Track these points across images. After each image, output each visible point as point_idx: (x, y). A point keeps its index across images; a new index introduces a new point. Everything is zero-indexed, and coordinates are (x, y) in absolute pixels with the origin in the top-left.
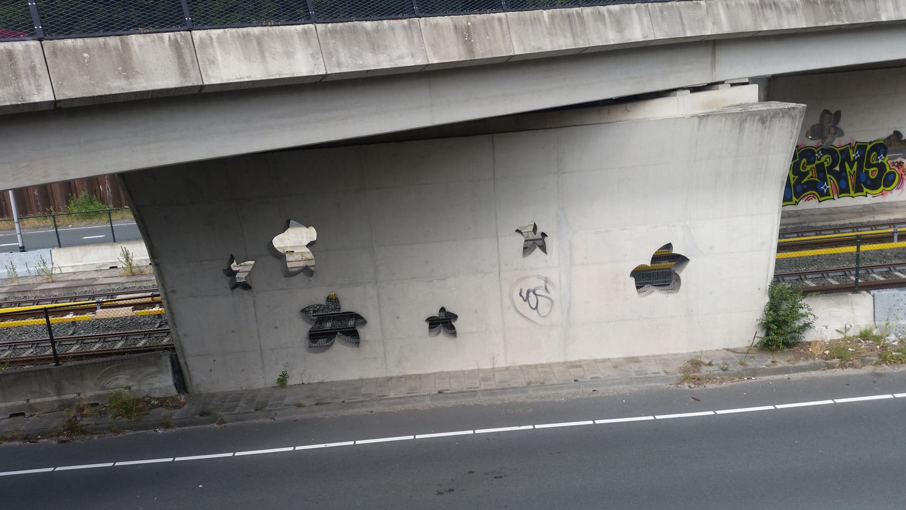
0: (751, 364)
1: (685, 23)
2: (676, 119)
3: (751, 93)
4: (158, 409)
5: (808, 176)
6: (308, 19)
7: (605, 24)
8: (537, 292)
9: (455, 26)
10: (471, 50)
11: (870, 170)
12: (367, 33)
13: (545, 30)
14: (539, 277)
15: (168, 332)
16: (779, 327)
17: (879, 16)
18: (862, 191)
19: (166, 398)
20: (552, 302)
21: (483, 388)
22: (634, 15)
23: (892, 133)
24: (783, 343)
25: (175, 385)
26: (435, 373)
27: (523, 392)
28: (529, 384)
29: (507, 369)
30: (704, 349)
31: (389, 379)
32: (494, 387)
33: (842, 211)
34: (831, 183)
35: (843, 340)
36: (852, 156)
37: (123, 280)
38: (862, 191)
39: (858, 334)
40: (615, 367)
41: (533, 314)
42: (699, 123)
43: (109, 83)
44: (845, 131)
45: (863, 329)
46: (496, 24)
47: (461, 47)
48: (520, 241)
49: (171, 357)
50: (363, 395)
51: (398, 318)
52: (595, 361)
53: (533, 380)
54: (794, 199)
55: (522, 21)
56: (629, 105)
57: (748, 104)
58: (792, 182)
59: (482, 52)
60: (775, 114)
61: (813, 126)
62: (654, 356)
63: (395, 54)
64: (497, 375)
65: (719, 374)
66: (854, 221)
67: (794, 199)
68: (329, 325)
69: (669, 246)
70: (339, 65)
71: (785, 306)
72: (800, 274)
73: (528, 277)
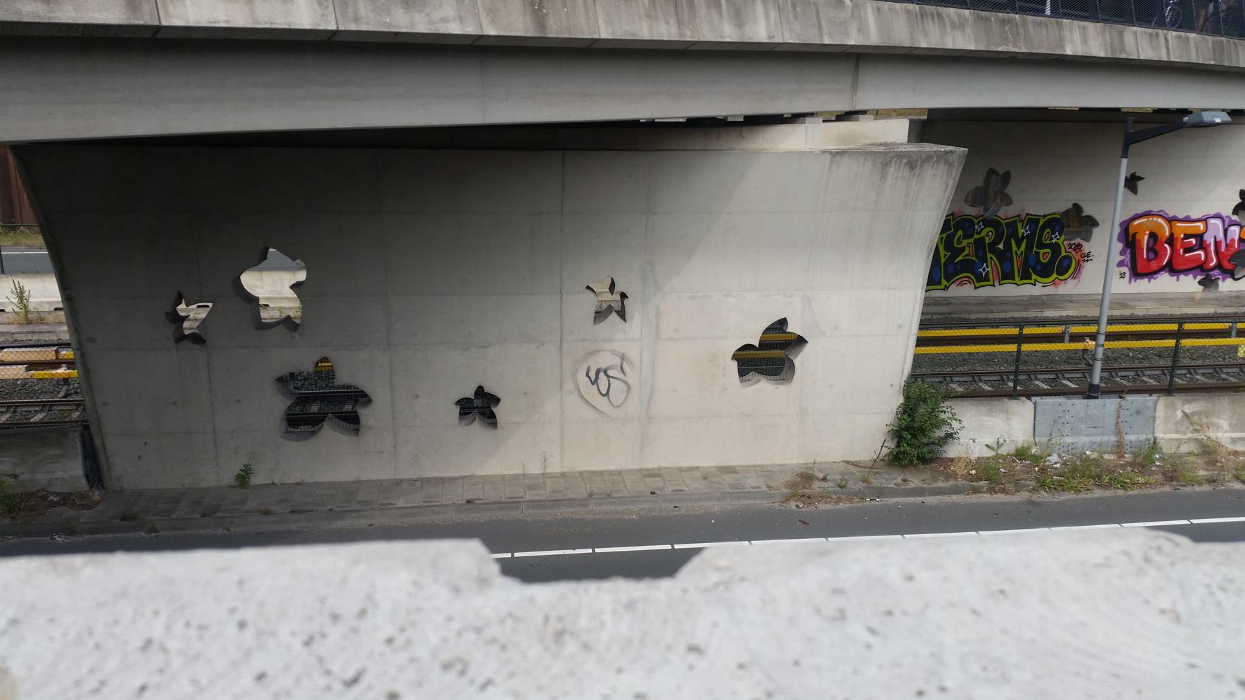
0: (876, 482)
2: (802, 154)
3: (898, 131)
4: (58, 509)
5: (964, 251)
8: (609, 373)
10: (541, 24)
11: (1042, 251)
13: (642, 11)
14: (613, 352)
15: (78, 404)
16: (914, 436)
17: (1063, 47)
18: (1030, 278)
19: (72, 494)
20: (629, 387)
21: (528, 498)
23: (1070, 206)
24: (918, 458)
25: (87, 475)
26: (464, 477)
27: (582, 505)
28: (591, 495)
29: (563, 475)
30: (819, 460)
31: (399, 482)
32: (544, 498)
34: (991, 266)
35: (993, 458)
36: (1021, 231)
37: (13, 329)
38: (1030, 278)
39: (1013, 451)
40: (705, 478)
41: (601, 402)
42: (831, 162)
43: (19, 5)
45: (1020, 446)
47: (528, 17)
48: (590, 304)
49: (82, 436)
50: (360, 502)
51: (417, 397)
52: (680, 469)
53: (596, 491)
54: (944, 282)
58: (943, 260)
60: (928, 158)
61: (976, 189)
62: (754, 466)
63: (437, 15)
64: (548, 481)
65: (835, 493)
66: (1017, 315)
67: (944, 282)
68: (314, 409)
69: (783, 322)
70: (357, 19)
71: (922, 410)
72: (944, 376)
73: (597, 351)
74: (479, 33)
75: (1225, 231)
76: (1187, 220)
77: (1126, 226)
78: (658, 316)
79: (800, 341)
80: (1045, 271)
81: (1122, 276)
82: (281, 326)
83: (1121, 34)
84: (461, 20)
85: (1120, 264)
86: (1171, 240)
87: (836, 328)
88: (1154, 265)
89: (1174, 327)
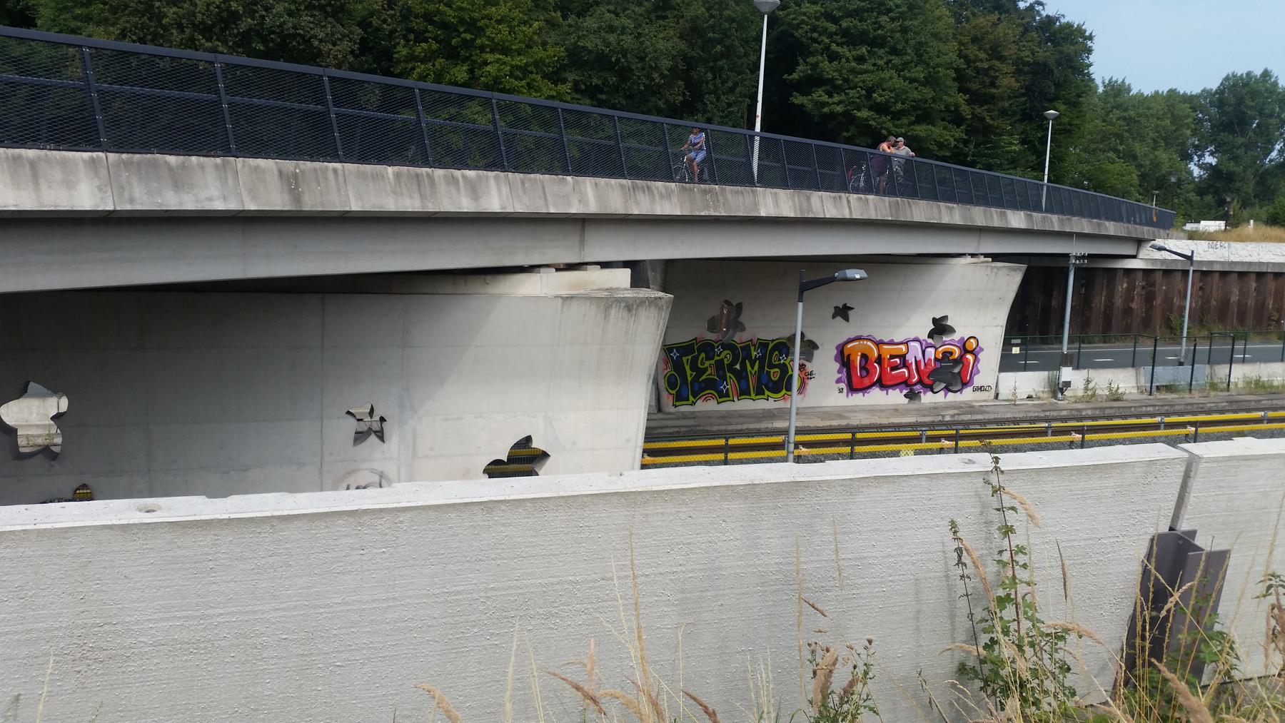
1: (549, 197)
3: (622, 277)
6: (96, 146)
7: (458, 189)
9: (280, 172)
10: (297, 199)
12: (170, 168)
14: (372, 471)
17: (758, 210)
22: (492, 184)
33: (741, 415)
34: (730, 384)
44: (746, 325)
46: (331, 175)
48: (351, 426)
54: (691, 398)
55: (362, 176)
56: (488, 277)
57: (618, 289)
59: (312, 202)
60: (642, 302)
63: (202, 195)
66: (751, 426)
67: (691, 398)
69: (529, 439)
70: (132, 201)
74: (241, 208)
75: (923, 352)
76: (892, 343)
77: (841, 349)
78: (415, 437)
79: (544, 455)
80: (776, 388)
81: (841, 391)
82: (40, 456)
83: (808, 198)
84: (225, 198)
85: (839, 381)
86: (879, 360)
87: (574, 443)
88: (867, 382)
89: (849, 436)
